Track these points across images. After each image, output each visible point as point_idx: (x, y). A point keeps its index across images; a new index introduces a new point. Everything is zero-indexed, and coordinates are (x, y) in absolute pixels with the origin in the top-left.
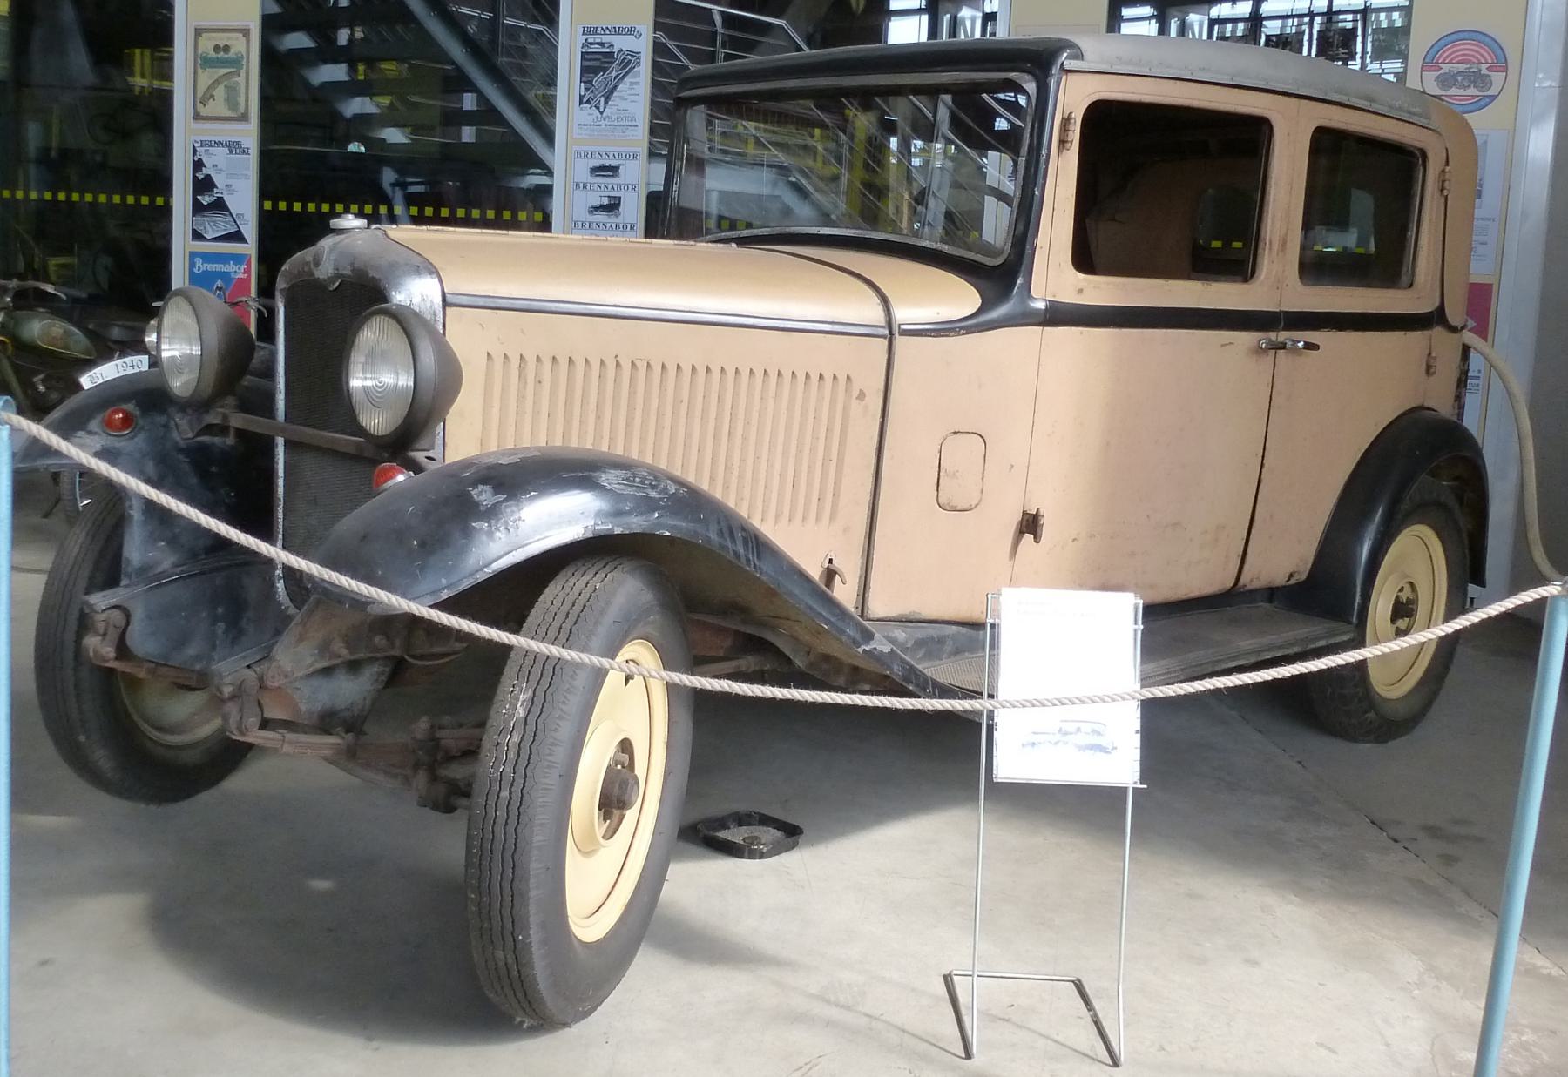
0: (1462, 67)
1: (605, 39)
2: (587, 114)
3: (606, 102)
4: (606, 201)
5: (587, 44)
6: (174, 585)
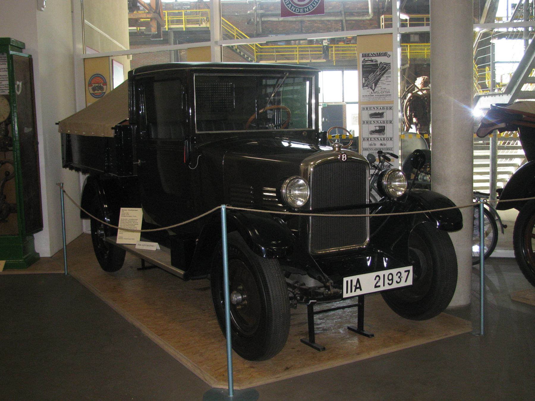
0: (97, 85)
1: (373, 58)
3: (375, 86)
4: (378, 128)
6: (478, 288)
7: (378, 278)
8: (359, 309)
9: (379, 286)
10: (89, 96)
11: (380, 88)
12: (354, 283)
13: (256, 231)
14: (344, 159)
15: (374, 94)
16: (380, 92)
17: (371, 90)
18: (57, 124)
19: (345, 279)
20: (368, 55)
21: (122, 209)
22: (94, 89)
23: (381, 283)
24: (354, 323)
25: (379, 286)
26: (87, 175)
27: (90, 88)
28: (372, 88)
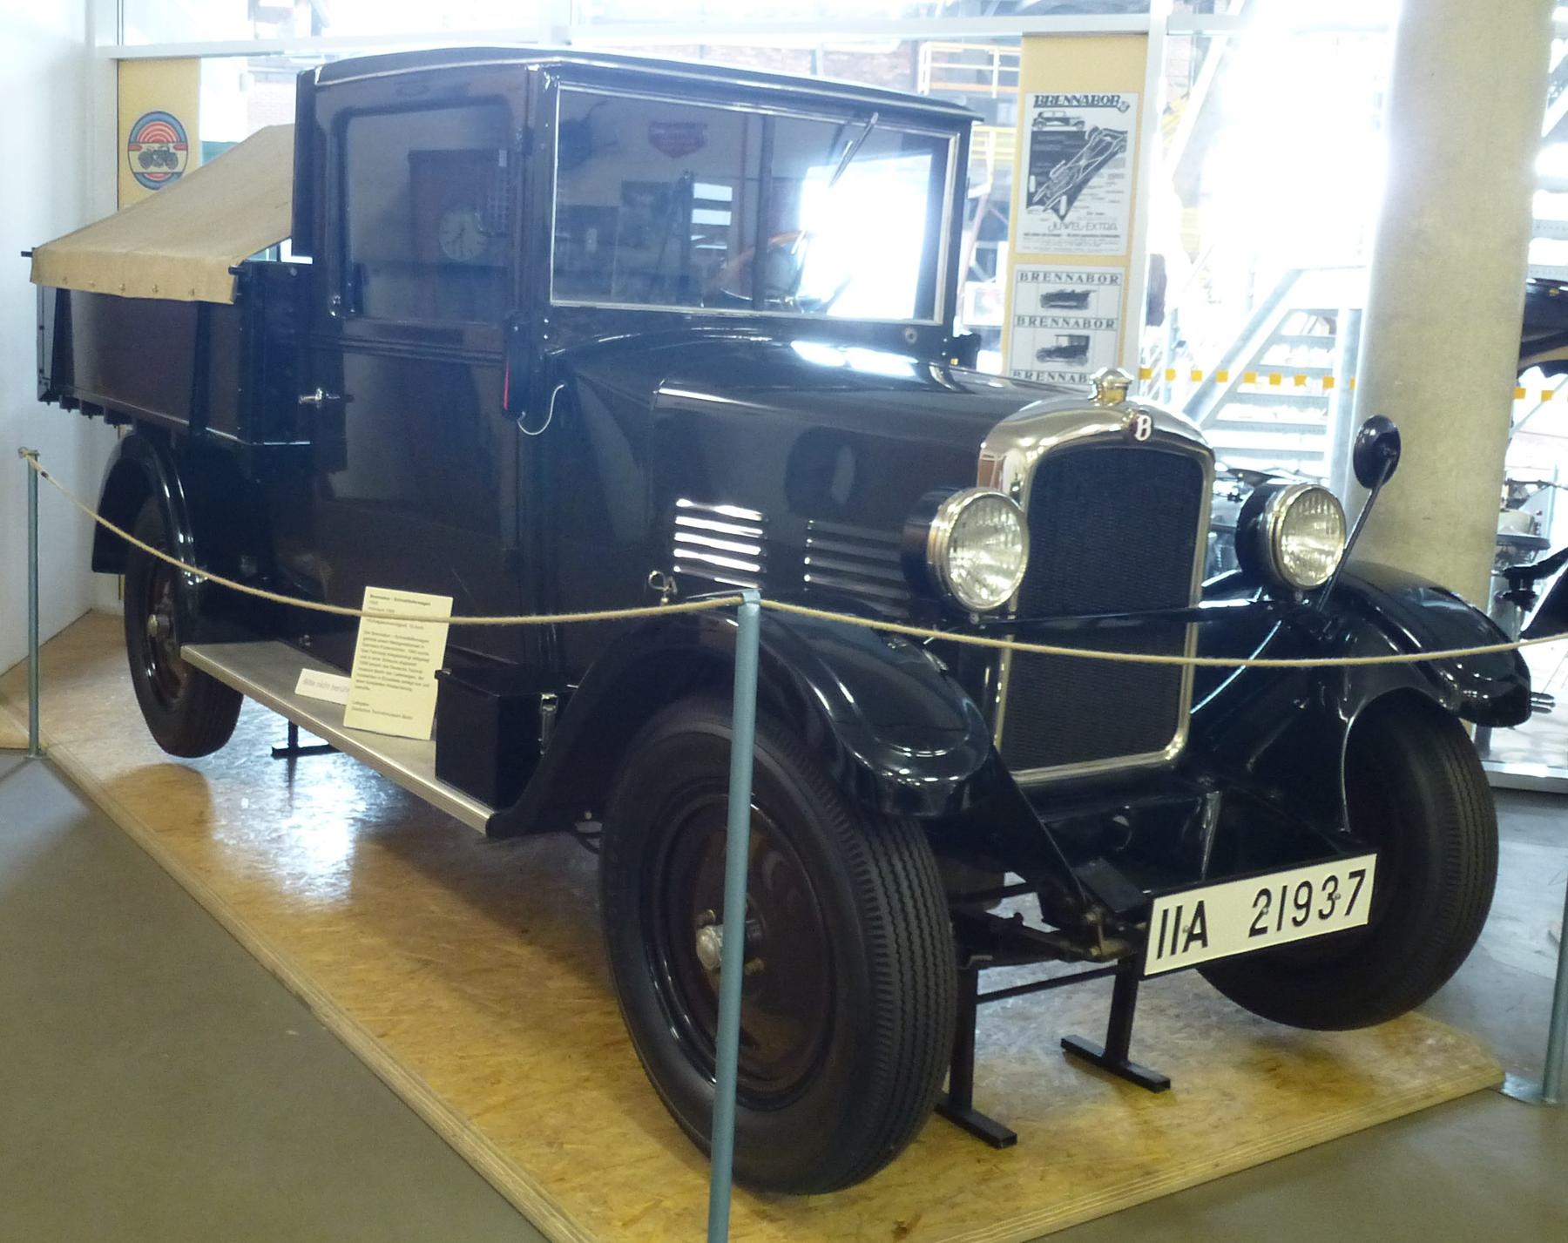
0: (156, 146)
1: (1071, 112)
2: (1041, 219)
3: (1070, 202)
4: (1064, 342)
5: (1040, 120)
7: (1263, 900)
8: (1117, 982)
9: (1264, 930)
10: (130, 182)
11: (1083, 212)
12: (1186, 920)
13: (850, 699)
14: (1144, 431)
15: (1064, 231)
16: (1083, 223)
17: (1055, 218)
18: (24, 254)
19: (1160, 905)
20: (1055, 102)
21: (369, 590)
22: (146, 160)
23: (1269, 921)
24: (1095, 1038)
25: (1264, 930)
26: (127, 428)
27: (135, 155)
28: (1056, 210)
